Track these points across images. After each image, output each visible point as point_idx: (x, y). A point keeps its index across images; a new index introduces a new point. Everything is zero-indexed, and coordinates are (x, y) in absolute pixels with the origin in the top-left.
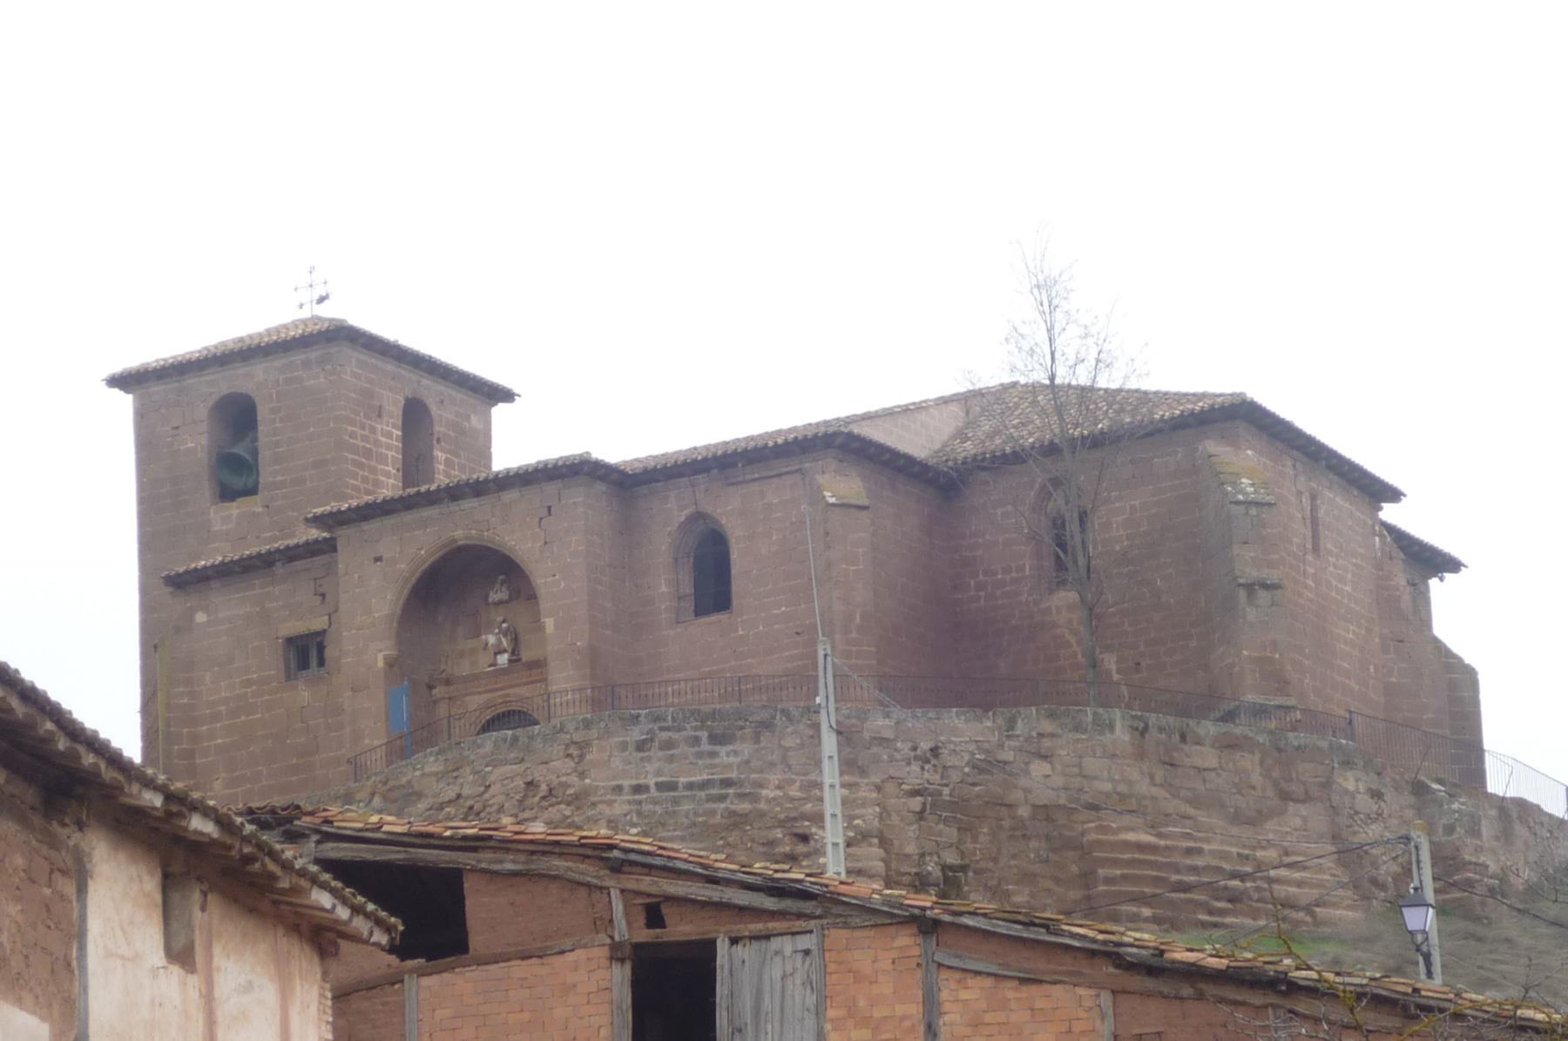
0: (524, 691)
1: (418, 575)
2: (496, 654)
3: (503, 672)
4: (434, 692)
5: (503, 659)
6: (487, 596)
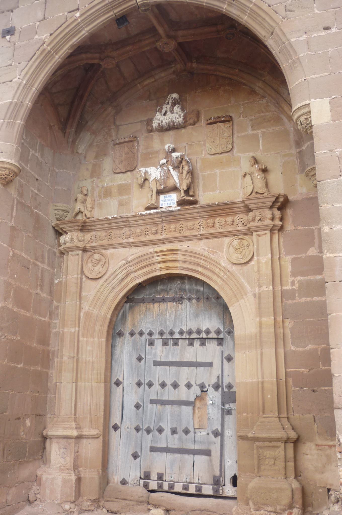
0: (200, 247)
1: (65, 51)
2: (159, 192)
3: (170, 216)
4: (62, 239)
5: (169, 202)
6: (150, 121)
